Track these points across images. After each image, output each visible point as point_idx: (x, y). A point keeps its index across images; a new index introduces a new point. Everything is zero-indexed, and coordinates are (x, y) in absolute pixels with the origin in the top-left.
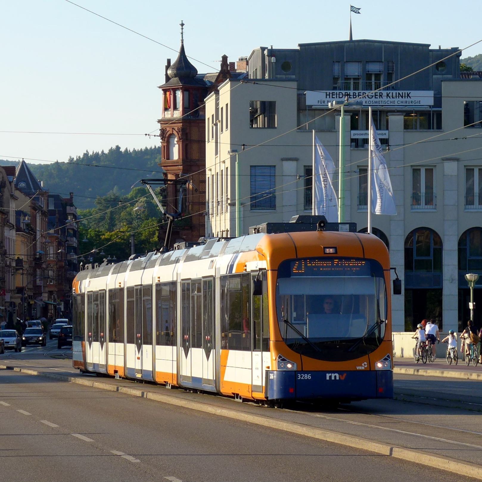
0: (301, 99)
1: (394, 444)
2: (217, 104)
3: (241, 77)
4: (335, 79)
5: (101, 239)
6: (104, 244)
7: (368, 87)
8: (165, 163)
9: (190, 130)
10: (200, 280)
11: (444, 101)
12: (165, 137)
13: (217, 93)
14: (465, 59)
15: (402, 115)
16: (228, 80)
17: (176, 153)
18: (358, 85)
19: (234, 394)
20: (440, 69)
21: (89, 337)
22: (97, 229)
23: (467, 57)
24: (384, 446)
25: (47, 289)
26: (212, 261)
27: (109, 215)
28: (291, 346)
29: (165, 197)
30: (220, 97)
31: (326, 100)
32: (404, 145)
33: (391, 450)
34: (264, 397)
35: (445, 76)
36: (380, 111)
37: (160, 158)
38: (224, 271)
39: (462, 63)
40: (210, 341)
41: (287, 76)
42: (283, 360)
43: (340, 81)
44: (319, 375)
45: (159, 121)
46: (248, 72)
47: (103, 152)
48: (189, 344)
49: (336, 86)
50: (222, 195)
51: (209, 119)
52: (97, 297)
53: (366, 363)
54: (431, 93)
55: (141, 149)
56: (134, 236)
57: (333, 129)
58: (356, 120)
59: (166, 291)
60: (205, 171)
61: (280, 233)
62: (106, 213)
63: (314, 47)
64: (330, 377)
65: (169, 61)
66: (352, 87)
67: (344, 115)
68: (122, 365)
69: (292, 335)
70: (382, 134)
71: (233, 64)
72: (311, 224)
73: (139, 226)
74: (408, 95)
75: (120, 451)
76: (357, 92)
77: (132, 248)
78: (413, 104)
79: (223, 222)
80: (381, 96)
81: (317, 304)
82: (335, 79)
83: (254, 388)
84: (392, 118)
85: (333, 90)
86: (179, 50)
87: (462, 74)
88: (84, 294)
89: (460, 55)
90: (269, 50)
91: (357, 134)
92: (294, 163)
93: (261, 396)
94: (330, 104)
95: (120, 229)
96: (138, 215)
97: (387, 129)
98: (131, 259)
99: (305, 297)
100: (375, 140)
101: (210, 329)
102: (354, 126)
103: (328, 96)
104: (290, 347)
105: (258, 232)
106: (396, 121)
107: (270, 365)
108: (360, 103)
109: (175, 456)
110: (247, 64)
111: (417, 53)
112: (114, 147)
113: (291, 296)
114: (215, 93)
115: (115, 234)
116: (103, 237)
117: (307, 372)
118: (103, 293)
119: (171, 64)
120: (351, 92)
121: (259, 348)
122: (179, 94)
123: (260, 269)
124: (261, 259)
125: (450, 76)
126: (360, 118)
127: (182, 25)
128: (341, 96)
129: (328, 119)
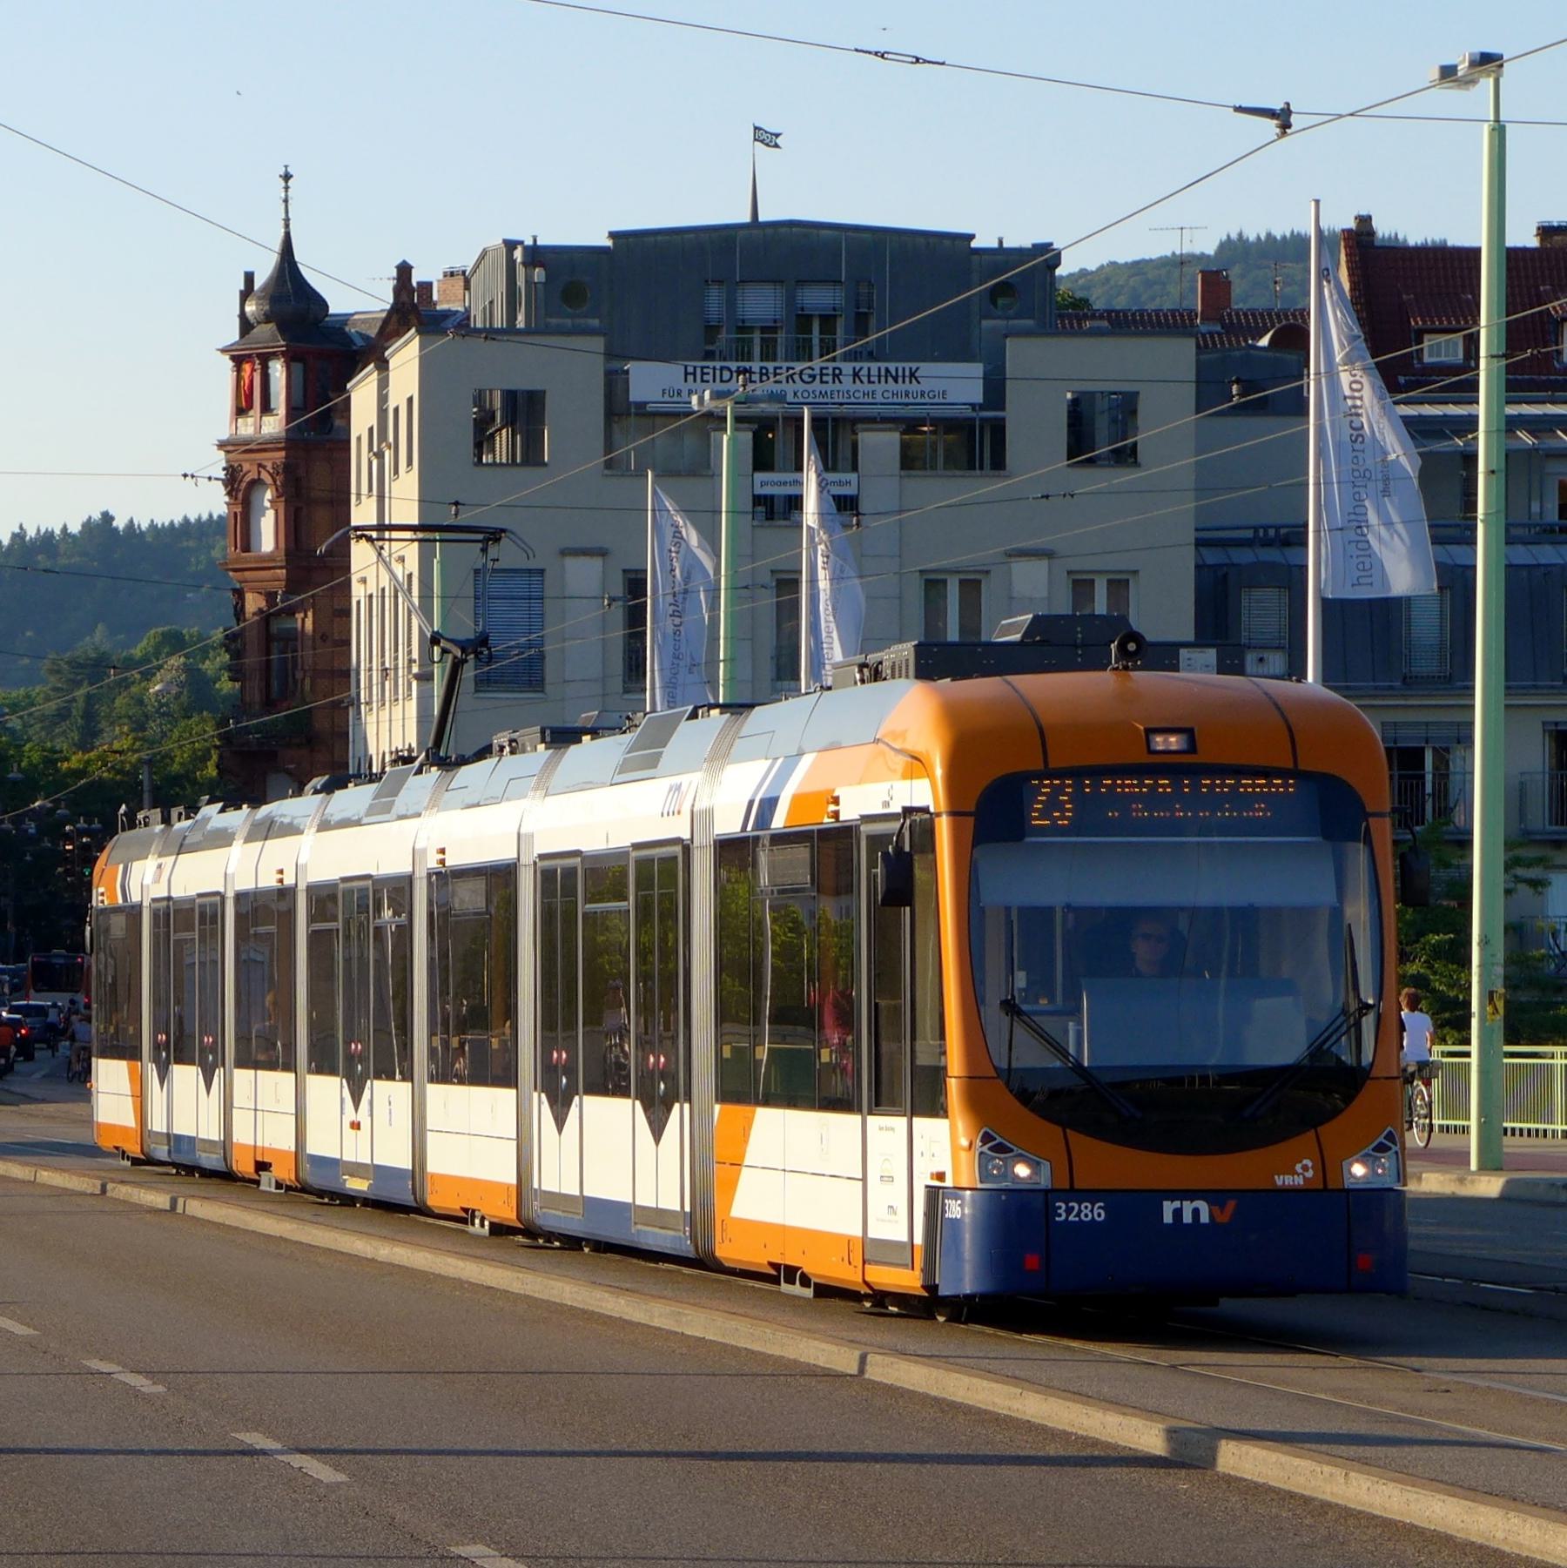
0: (615, 384)
1: (872, 1345)
2: (383, 399)
3: (449, 323)
4: (711, 331)
5: (57, 770)
6: (67, 786)
7: (802, 351)
8: (237, 560)
9: (307, 467)
10: (621, 854)
11: (1013, 392)
12: (238, 490)
13: (383, 365)
14: (1071, 275)
15: (895, 430)
16: (413, 330)
17: (268, 534)
18: (775, 347)
19: (775, 1266)
20: (1000, 302)
21: (157, 1047)
22: (49, 744)
23: (1075, 269)
24: (843, 1349)
26: (678, 787)
27: (81, 703)
28: (1024, 1097)
29: (237, 655)
30: (392, 375)
31: (685, 388)
32: (901, 512)
33: (863, 1360)
34: (919, 1284)
35: (1016, 322)
36: (836, 420)
37: (225, 549)
38: (729, 823)
39: (1062, 288)
40: (213, 1049)
41: (578, 321)
42: (1000, 1149)
43: (723, 335)
44: (1133, 1207)
45: (222, 445)
46: (468, 310)
47: (65, 528)
48: (215, 1058)
49: (711, 348)
50: (396, 650)
51: (359, 439)
52: (187, 920)
53: (1307, 1162)
54: (977, 369)
55: (172, 523)
56: (150, 762)
57: (704, 467)
58: (769, 444)
59: (350, 908)
60: (347, 585)
61: (984, 676)
62: (74, 700)
63: (652, 239)
64: (1178, 1213)
65: (249, 278)
66: (757, 350)
67: (735, 429)
68: (289, 1144)
69: (1031, 1055)
70: (840, 483)
71: (426, 287)
72: (1076, 646)
73: (164, 734)
74: (912, 375)
75: (111, 1360)
76: (770, 365)
77: (146, 796)
78: (927, 400)
79: (397, 725)
80: (837, 376)
81: (1105, 943)
82: (711, 331)
83: (873, 1250)
84: (869, 439)
85: (705, 359)
86: (277, 245)
87: (1061, 317)
88: (140, 905)
89: (1058, 264)
90: (526, 249)
91: (771, 483)
92: (596, 563)
93: (908, 1280)
94: (695, 399)
95: (111, 744)
96: (161, 705)
97: (855, 468)
98: (316, 792)
100: (820, 499)
101: (213, 1023)
102: (763, 459)
103: (690, 378)
104: (1020, 1101)
105: (877, 675)
106: (880, 445)
107: (946, 1166)
108: (779, 398)
109: (263, 1376)
110: (467, 286)
111: (936, 260)
112: (97, 516)
113: (1008, 909)
114: (377, 368)
115: (99, 758)
116: (66, 765)
117: (1091, 1195)
118: (214, 905)
119: (257, 287)
120: (756, 366)
121: (893, 1103)
122: (278, 370)
123: (908, 811)
124: (909, 775)
125: (1029, 323)
126: (780, 439)
127: (287, 177)
128: (726, 375)
129: (690, 441)
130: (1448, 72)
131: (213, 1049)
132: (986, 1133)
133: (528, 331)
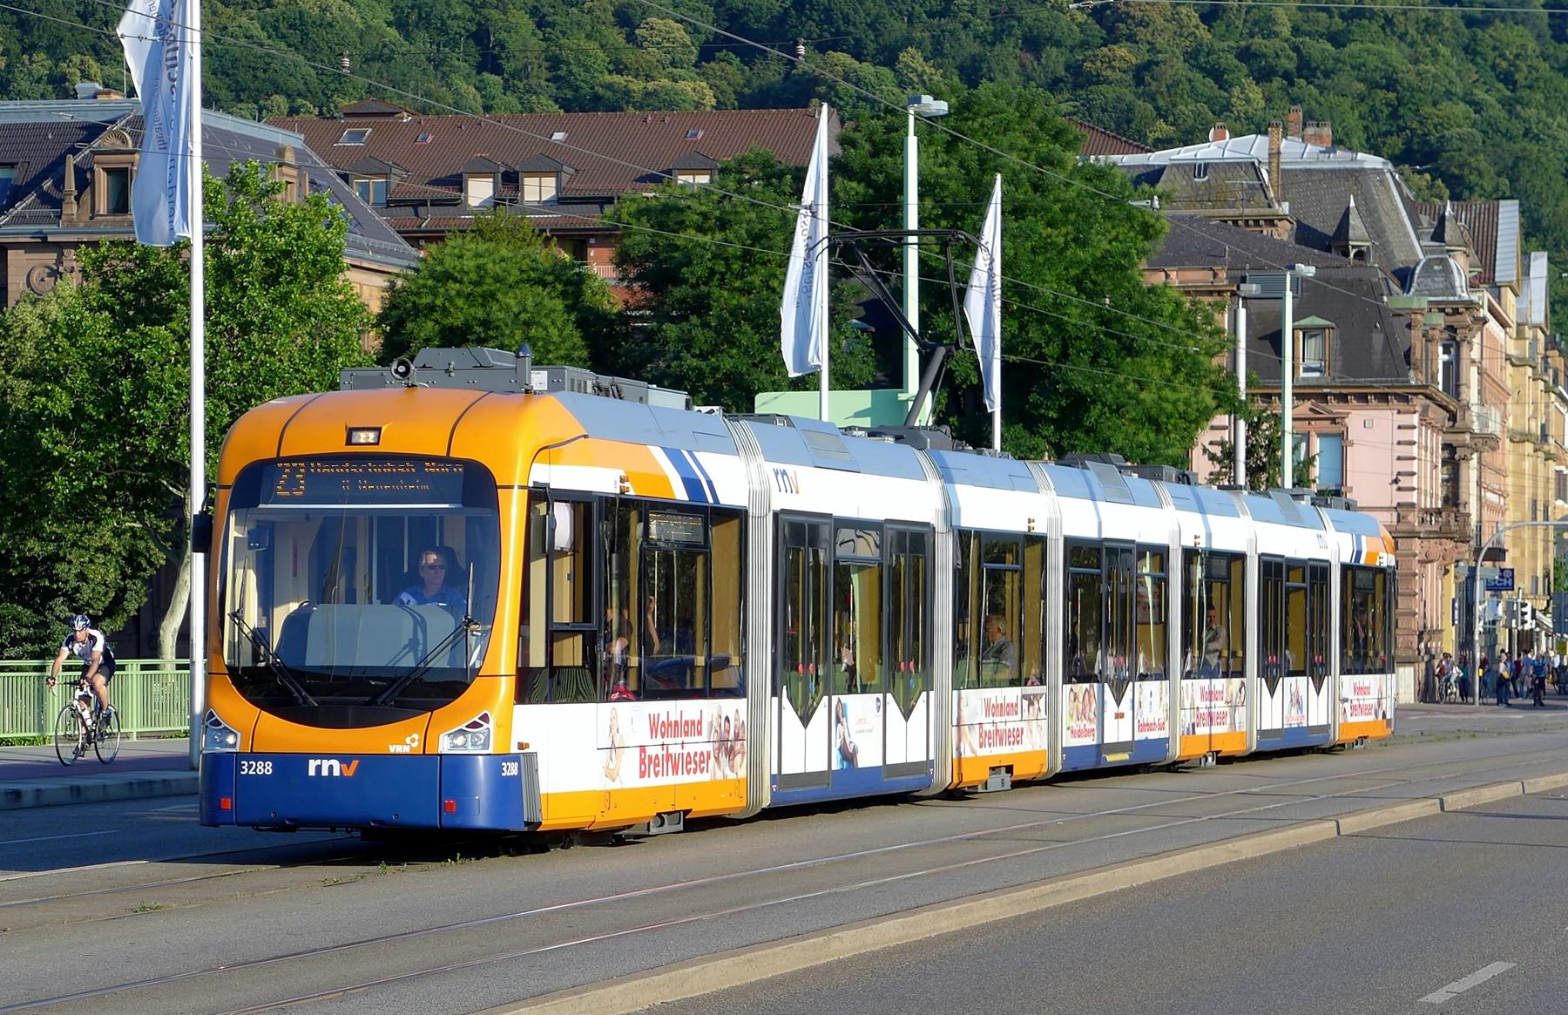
64: (319, 768)
99: (1056, 556)
117: (263, 757)
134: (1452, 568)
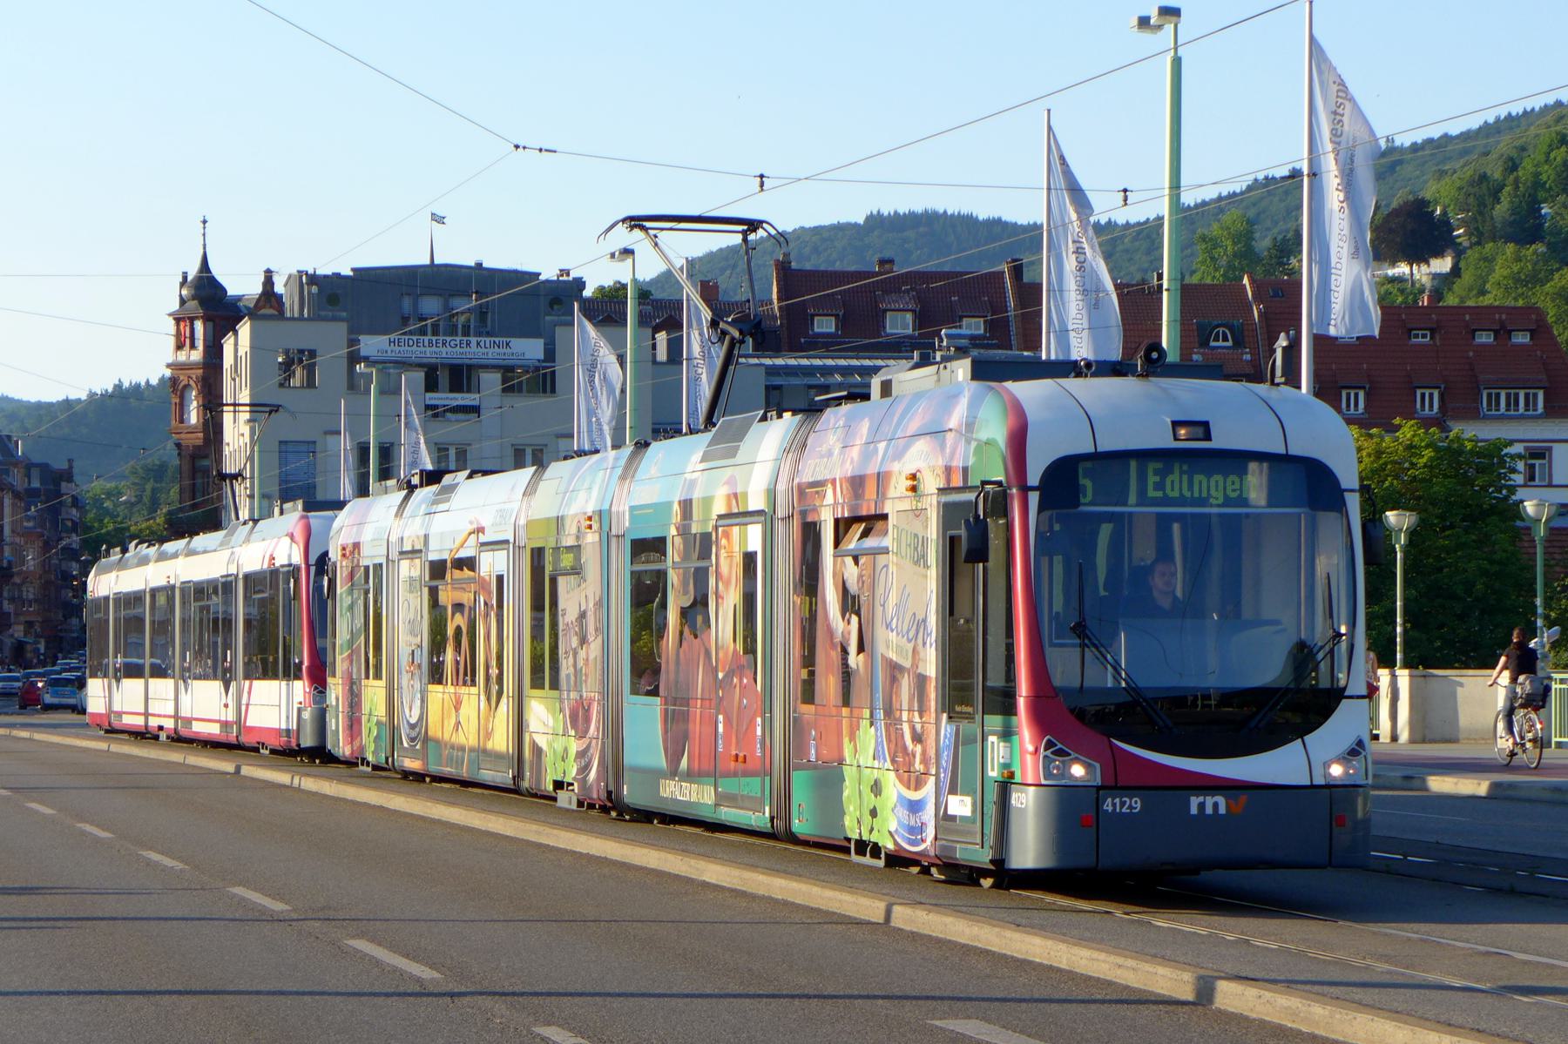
13: (236, 333)
25: (22, 619)
28: (1080, 715)
64: (1202, 806)
80: (468, 344)
127: (205, 222)
130: (1144, 22)
131: (229, 670)
132: (1049, 742)
133: (309, 319)
134: (417, 672)
